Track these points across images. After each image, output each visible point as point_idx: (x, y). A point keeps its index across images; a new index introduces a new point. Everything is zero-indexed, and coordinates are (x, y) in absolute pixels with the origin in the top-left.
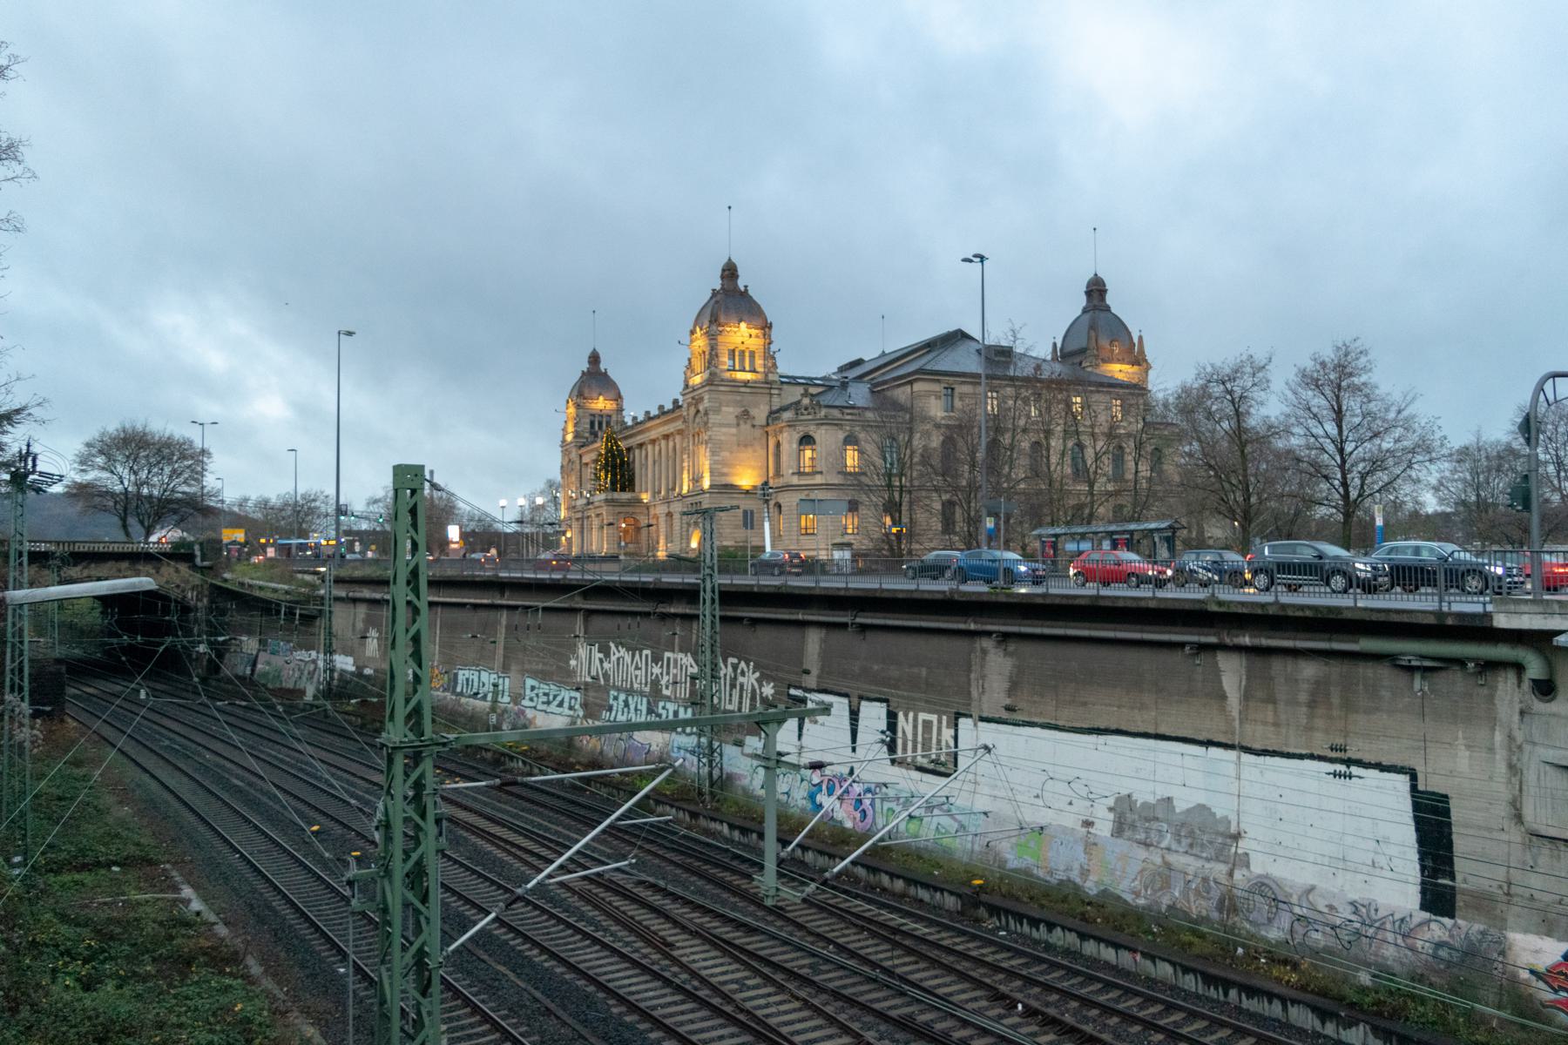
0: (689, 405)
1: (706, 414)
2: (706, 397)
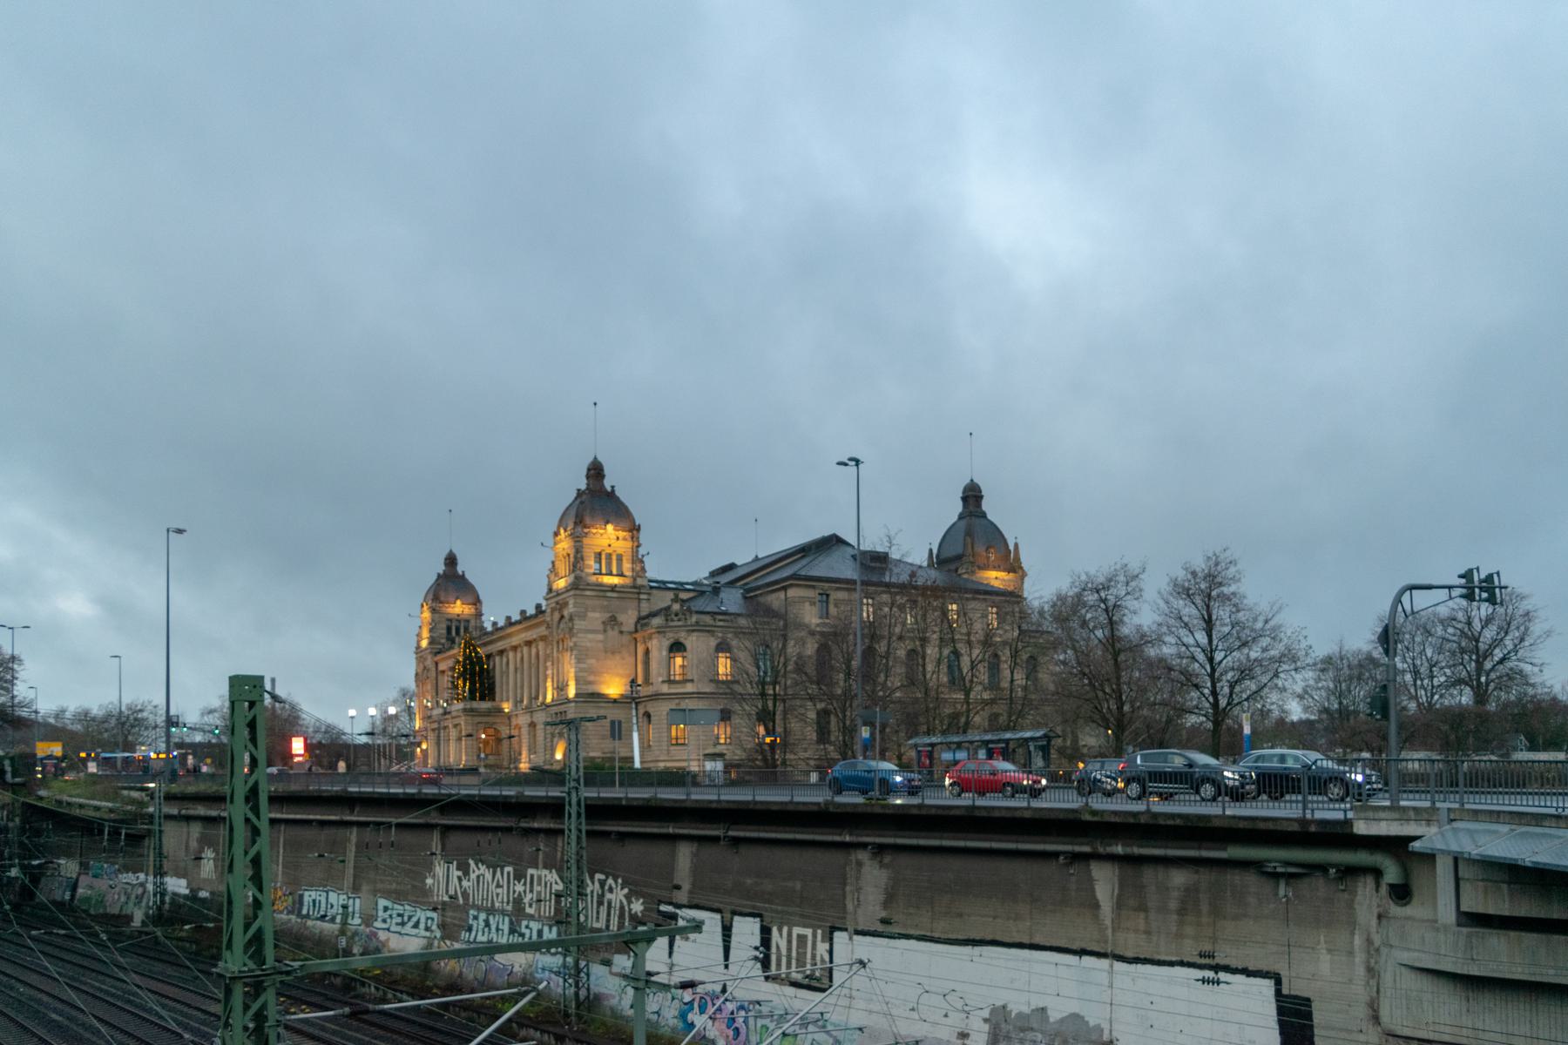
0: (553, 610)
1: (571, 619)
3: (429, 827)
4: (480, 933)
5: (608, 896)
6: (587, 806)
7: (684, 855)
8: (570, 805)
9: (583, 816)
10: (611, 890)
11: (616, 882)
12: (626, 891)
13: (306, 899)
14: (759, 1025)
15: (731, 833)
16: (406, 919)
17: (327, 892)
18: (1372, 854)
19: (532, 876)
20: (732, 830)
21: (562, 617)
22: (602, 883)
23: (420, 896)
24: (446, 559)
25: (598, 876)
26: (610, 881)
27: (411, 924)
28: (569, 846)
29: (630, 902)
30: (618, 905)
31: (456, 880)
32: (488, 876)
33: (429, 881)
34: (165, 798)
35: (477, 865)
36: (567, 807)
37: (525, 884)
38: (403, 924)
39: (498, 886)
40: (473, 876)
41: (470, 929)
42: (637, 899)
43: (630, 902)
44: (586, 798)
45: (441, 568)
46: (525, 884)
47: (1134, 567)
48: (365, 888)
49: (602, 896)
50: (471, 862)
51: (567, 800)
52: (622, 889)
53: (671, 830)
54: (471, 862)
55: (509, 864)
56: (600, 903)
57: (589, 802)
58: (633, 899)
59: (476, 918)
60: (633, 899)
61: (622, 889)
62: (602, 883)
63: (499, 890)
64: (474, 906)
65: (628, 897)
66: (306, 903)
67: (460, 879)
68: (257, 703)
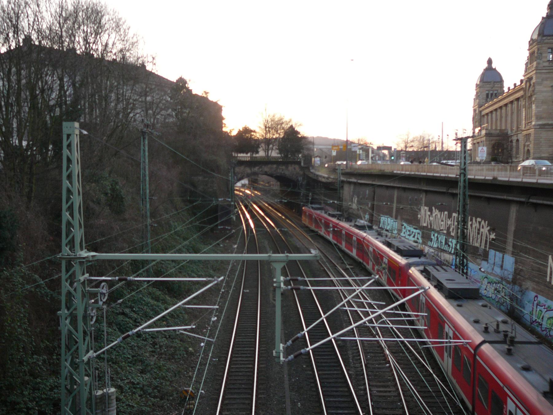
0: (526, 82)
1: (534, 86)
2: (534, 78)
3: (420, 191)
4: (435, 243)
5: (481, 230)
6: (469, 183)
7: (513, 211)
8: (460, 182)
9: (467, 188)
10: (483, 227)
11: (485, 223)
12: (489, 228)
13: (382, 221)
14: (538, 310)
15: (531, 200)
16: (411, 233)
17: (387, 218)
18: (495, 179)
19: (454, 217)
20: (532, 199)
21: (530, 85)
22: (480, 223)
23: (414, 221)
24: (488, 61)
25: (479, 219)
26: (483, 222)
27: (412, 235)
28: (458, 203)
29: (490, 234)
30: (485, 234)
31: (428, 217)
32: (439, 216)
33: (419, 216)
34: (342, 174)
35: (435, 209)
36: (459, 183)
37: (451, 221)
38: (410, 235)
39: (442, 221)
40: (434, 215)
41: (431, 241)
42: (493, 233)
43: (490, 234)
44: (469, 179)
45: (485, 65)
46: (451, 221)
47: (226, 126)
48: (399, 217)
49: (479, 230)
50: (433, 208)
51: (459, 179)
52: (487, 227)
53: (505, 197)
54: (433, 208)
55: (446, 211)
56: (478, 233)
57: (470, 181)
58: (491, 233)
59: (434, 235)
60: (491, 233)
61: (487, 227)
62: (480, 223)
63: (442, 223)
64: (434, 230)
65: (489, 231)
66: (381, 222)
67: (429, 216)
68: (72, 135)
